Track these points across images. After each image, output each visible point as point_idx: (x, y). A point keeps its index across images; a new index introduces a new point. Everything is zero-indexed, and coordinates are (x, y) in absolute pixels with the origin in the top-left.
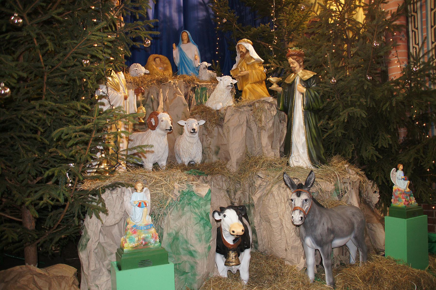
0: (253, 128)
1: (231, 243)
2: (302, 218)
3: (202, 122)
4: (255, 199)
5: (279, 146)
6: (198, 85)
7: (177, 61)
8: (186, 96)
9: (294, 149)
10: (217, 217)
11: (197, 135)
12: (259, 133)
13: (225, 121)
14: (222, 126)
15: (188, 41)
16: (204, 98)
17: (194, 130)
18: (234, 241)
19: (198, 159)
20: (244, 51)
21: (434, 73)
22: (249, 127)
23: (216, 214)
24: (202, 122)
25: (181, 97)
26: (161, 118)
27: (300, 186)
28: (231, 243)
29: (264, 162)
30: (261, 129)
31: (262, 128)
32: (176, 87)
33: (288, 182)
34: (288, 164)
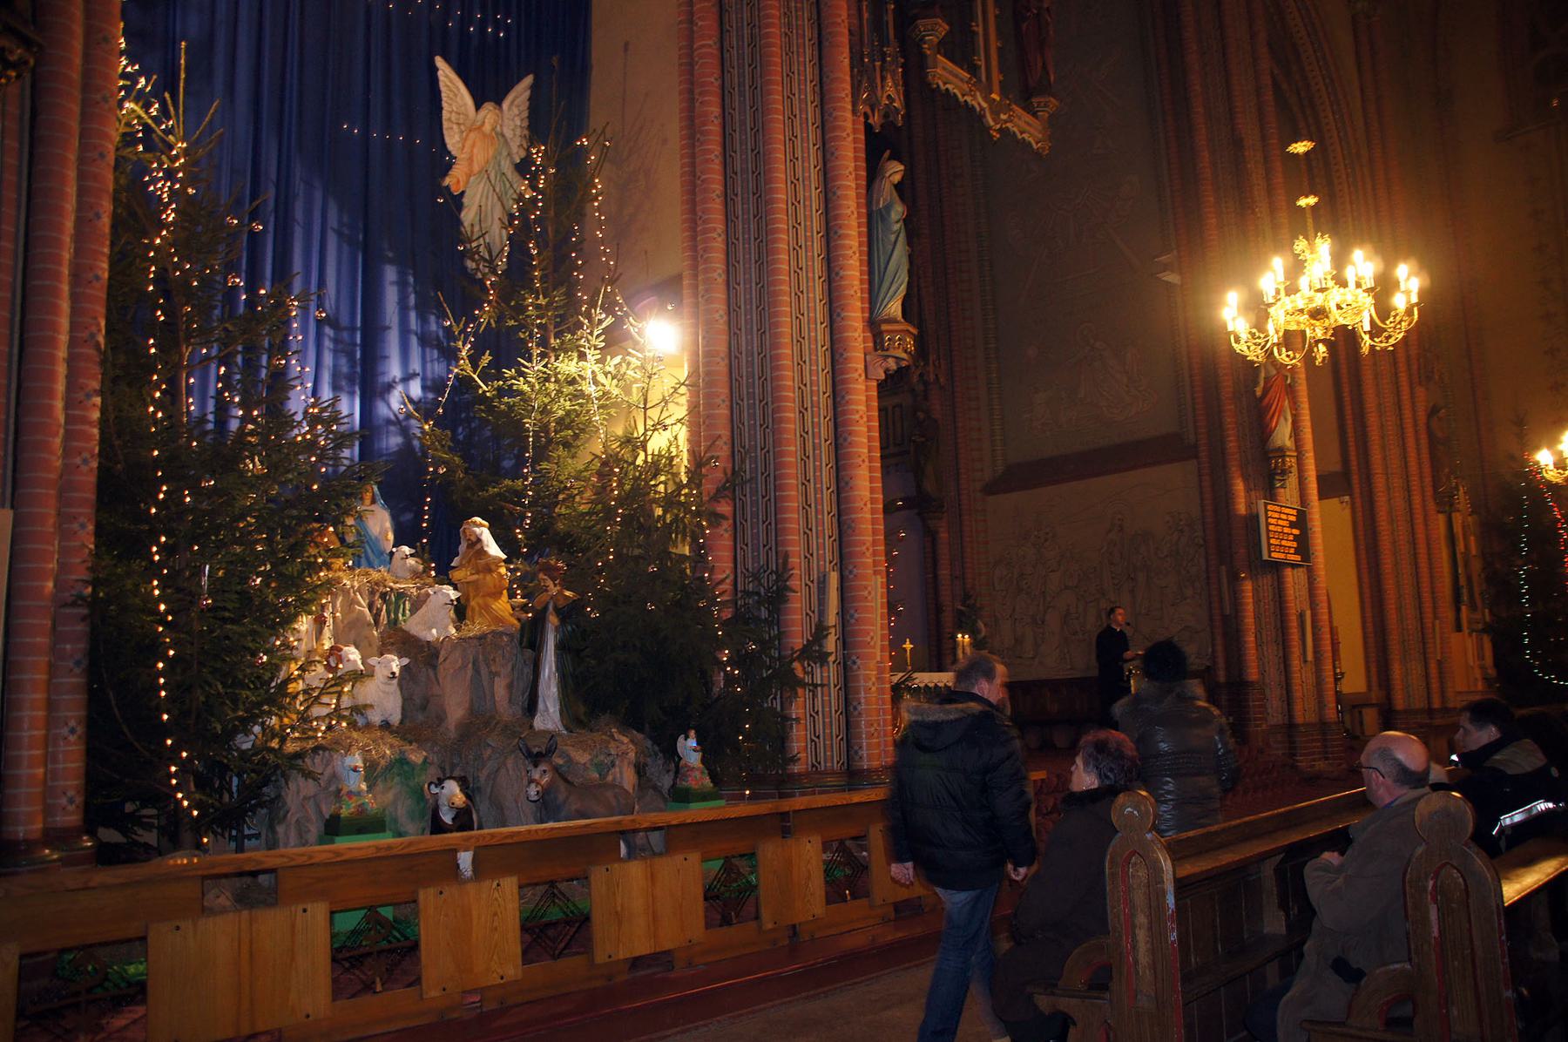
0: (482, 672)
1: (450, 823)
2: (538, 792)
3: (406, 661)
4: (483, 775)
5: (522, 699)
6: (392, 589)
7: (649, 869)
8: (370, 606)
9: (541, 706)
10: (434, 790)
11: (395, 681)
12: (492, 682)
13: (441, 659)
14: (434, 667)
15: (373, 501)
16: (401, 610)
17: (393, 673)
18: (453, 819)
19: (396, 718)
20: (473, 538)
21: (326, 788)
22: (477, 671)
23: (433, 787)
24: (406, 661)
25: (363, 612)
26: (347, 656)
27: (539, 755)
28: (450, 823)
29: (496, 724)
30: (493, 675)
31: (497, 674)
32: (354, 593)
33: (524, 750)
34: (531, 727)
